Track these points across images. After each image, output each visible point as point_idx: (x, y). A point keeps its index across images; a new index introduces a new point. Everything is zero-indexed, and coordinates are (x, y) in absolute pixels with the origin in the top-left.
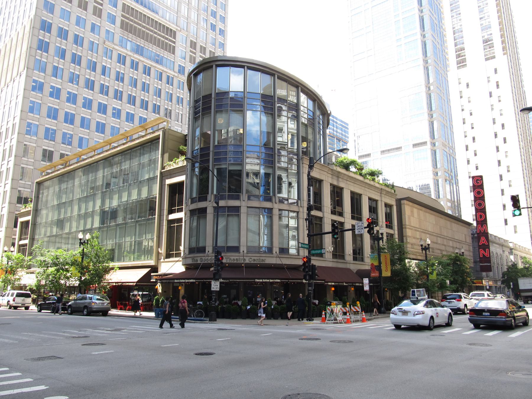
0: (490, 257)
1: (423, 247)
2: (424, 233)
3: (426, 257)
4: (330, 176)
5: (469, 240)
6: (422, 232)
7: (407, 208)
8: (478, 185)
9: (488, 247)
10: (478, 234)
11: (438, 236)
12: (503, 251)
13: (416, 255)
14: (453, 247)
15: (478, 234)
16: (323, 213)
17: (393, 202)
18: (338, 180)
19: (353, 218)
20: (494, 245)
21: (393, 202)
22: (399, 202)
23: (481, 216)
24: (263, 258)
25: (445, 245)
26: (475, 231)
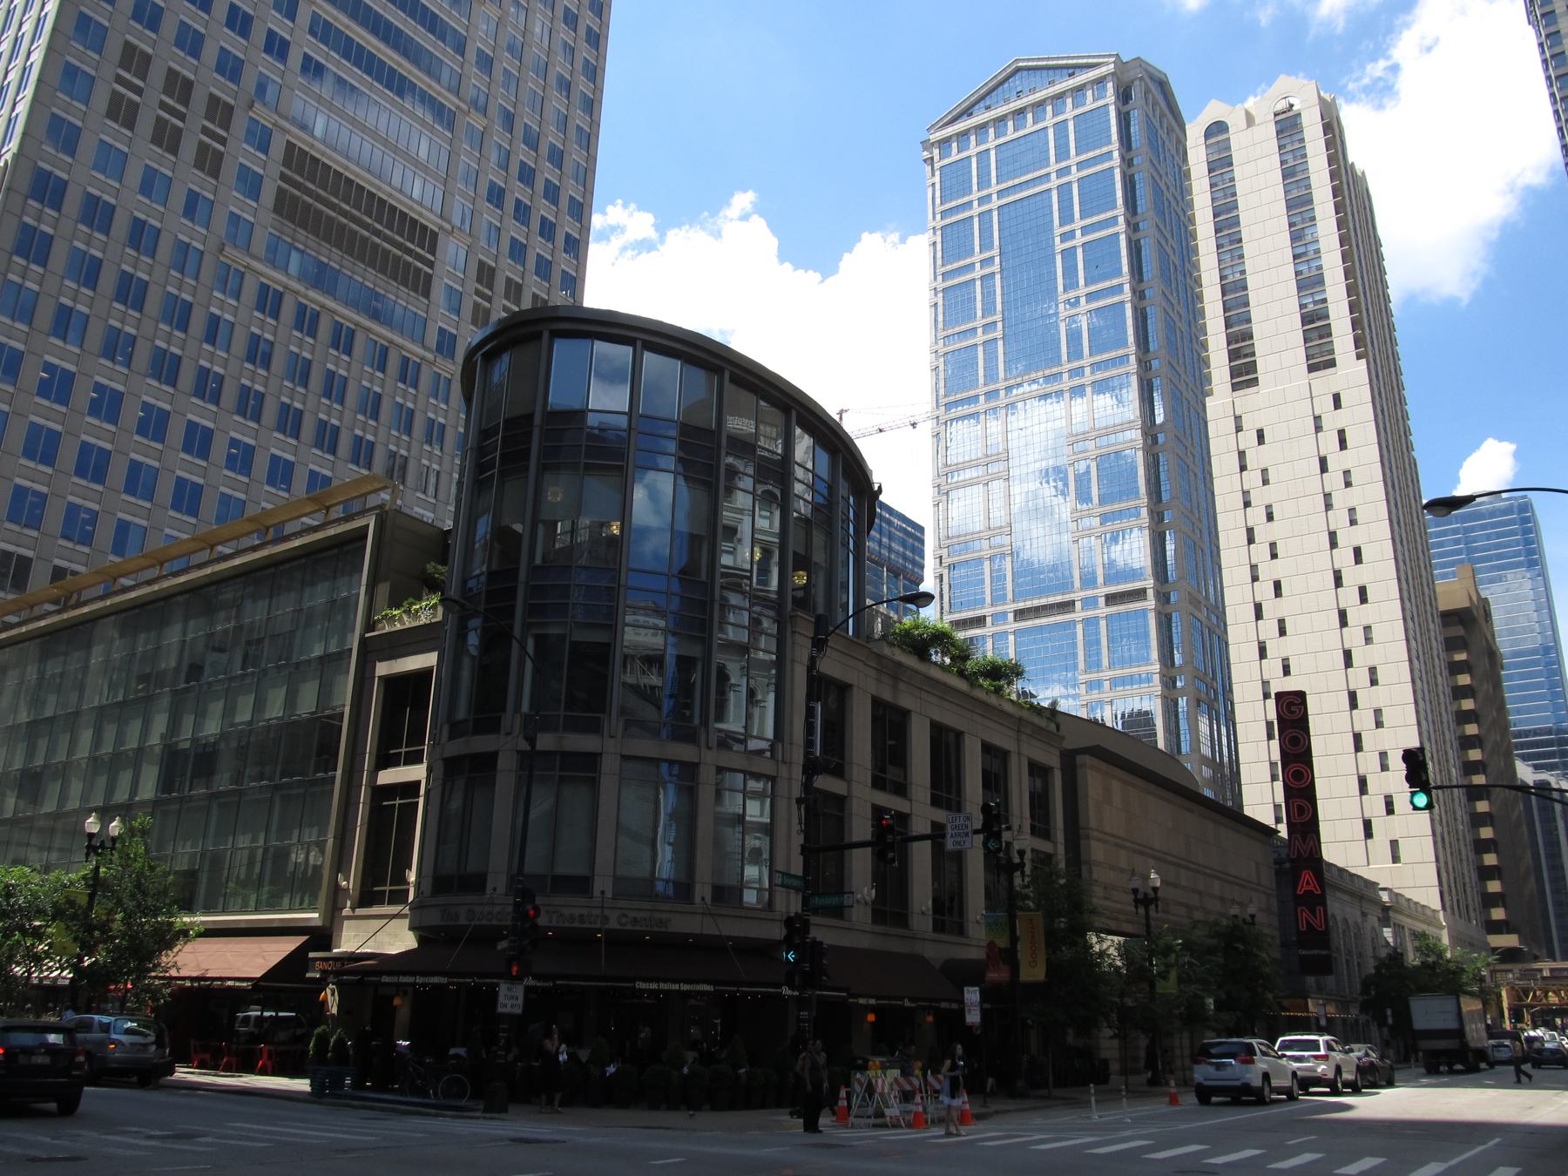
0: (1326, 933)
1: (1140, 896)
2: (1142, 854)
3: (1148, 926)
4: (873, 673)
5: (1268, 879)
6: (1171, 863)
7: (1094, 780)
8: (1292, 715)
9: (1321, 900)
10: (1292, 861)
11: (1179, 865)
12: (1364, 915)
13: (1116, 919)
14: (1222, 899)
15: (1292, 861)
16: (849, 782)
17: (1052, 760)
18: (895, 688)
19: (936, 802)
20: (1339, 894)
21: (1052, 760)
22: (1069, 759)
23: (1301, 810)
24: (664, 916)
25: (1200, 893)
26: (1284, 852)
